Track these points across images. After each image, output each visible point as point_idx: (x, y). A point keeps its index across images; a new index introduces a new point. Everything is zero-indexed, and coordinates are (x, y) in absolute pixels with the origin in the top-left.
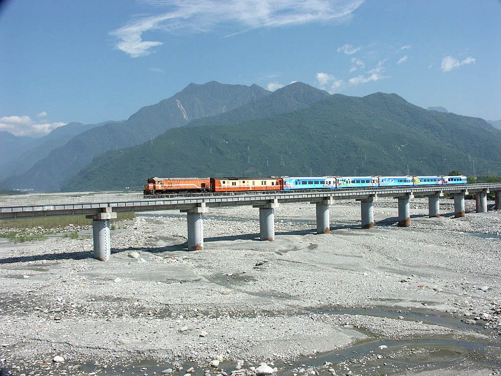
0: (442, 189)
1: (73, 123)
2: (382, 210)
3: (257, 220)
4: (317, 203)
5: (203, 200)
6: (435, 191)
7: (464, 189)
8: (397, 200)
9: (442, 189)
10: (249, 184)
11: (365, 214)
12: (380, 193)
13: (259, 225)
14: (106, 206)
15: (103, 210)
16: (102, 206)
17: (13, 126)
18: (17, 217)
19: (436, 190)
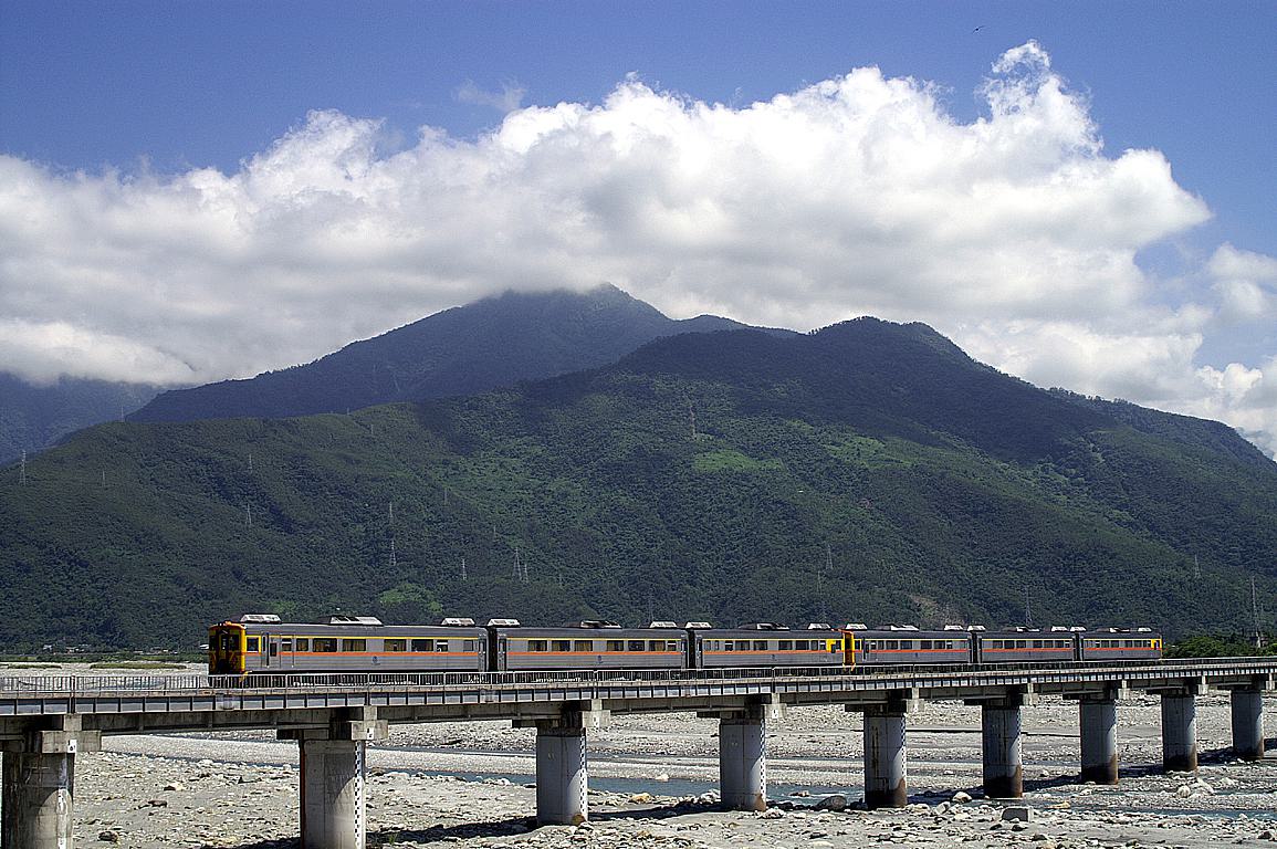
0: (1205, 673)
1: (554, 131)
2: (404, 788)
3: (711, 755)
4: (538, 724)
5: (773, 685)
6: (1180, 678)
7: (1113, 677)
8: (529, 734)
9: (1205, 673)
10: (265, 617)
11: (878, 760)
12: (928, 685)
13: (1161, 738)
14: (61, 710)
15: (53, 723)
16: (50, 710)
17: (983, 327)
18: (214, 726)
19: (1107, 678)
